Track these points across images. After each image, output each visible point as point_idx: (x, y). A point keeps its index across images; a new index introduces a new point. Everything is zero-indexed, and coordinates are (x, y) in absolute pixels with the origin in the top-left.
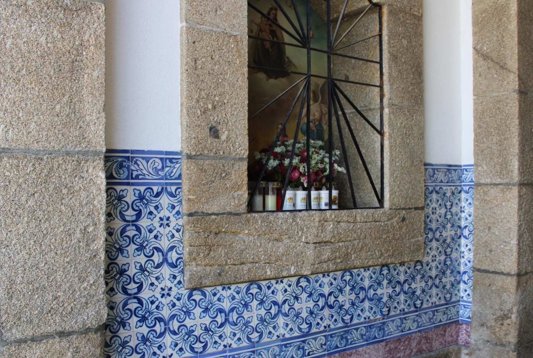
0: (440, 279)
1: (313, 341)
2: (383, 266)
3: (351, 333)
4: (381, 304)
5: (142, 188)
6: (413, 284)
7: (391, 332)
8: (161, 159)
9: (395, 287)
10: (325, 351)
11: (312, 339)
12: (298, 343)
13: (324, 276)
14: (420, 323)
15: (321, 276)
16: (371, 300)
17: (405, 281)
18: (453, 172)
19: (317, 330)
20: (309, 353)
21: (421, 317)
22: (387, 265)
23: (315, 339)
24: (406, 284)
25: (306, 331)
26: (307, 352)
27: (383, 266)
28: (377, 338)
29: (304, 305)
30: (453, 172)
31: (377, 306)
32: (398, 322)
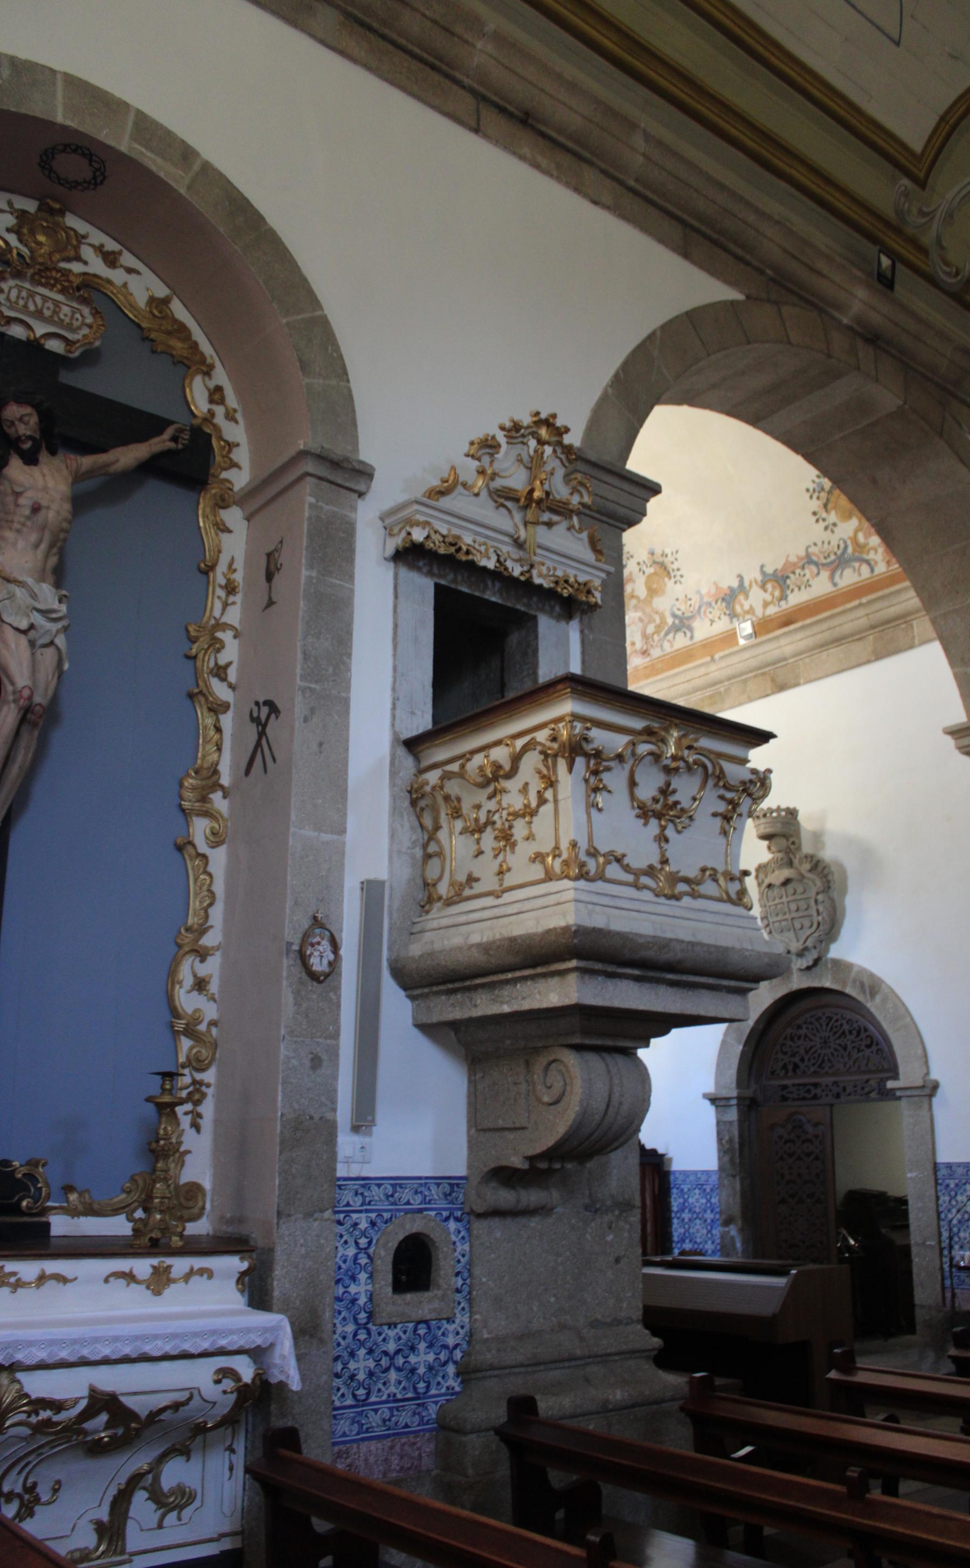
0: (344, 1364)
1: (373, 1413)
2: (419, 1322)
3: (366, 1416)
4: (415, 1378)
5: (373, 1215)
6: (352, 1362)
7: (372, 1427)
8: (392, 1185)
9: (439, 1353)
10: (389, 1429)
11: (372, 1410)
12: (352, 1415)
13: (389, 1328)
14: (365, 1427)
15: (386, 1327)
16: (399, 1369)
17: (398, 1352)
18: (374, 1188)
19: (378, 1399)
20: (367, 1429)
21: (426, 1409)
22: (426, 1322)
23: (376, 1411)
24: (400, 1357)
25: (421, 1391)
26: (426, 1419)
27: (419, 1322)
28: (347, 1436)
29: (361, 1365)
30: (374, 1188)
31: (348, 1386)
32: (387, 1414)
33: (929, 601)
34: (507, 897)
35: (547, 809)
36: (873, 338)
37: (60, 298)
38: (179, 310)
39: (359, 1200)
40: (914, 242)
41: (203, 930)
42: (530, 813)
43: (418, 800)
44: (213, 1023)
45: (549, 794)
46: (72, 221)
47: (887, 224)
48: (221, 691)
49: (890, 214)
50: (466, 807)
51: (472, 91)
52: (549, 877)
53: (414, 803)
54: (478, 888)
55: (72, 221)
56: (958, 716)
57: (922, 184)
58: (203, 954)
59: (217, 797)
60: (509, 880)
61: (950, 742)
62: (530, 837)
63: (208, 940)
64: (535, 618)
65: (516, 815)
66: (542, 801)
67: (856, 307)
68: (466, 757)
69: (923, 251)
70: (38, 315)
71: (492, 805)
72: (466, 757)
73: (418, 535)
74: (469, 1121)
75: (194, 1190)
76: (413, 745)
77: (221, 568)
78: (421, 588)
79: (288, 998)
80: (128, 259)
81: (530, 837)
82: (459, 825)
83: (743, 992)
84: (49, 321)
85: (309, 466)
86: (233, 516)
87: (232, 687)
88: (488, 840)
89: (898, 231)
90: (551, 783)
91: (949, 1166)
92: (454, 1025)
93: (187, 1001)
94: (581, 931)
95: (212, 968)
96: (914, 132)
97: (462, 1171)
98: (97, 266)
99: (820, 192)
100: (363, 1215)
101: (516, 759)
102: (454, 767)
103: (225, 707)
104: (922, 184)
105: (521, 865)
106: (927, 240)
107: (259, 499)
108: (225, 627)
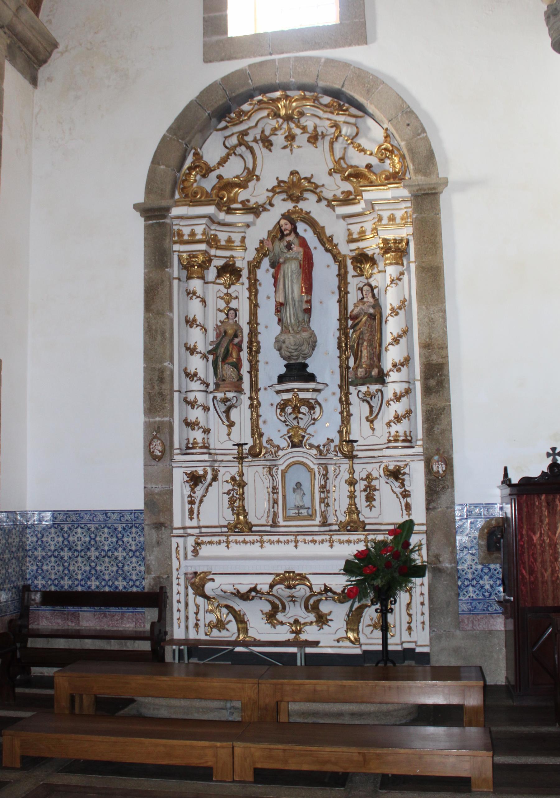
5: (124, 525)
8: (94, 521)
39: (136, 515)
100: (93, 525)
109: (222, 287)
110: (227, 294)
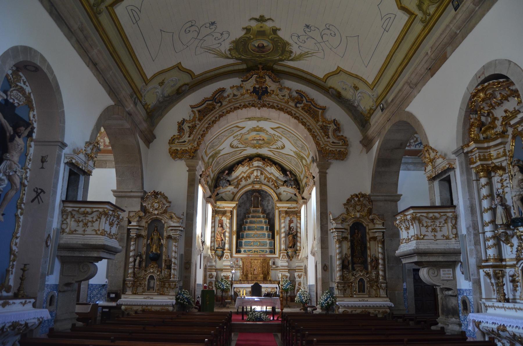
33: (117, 162)
34: (86, 236)
35: (98, 222)
36: (130, 114)
37: (21, 95)
38: (32, 97)
40: (141, 95)
41: (17, 233)
42: (93, 222)
43: (63, 212)
44: (17, 252)
45: (99, 220)
46: (20, 74)
47: (138, 90)
48: (26, 183)
49: (140, 89)
50: (75, 217)
51: (89, 58)
52: (97, 234)
53: (62, 212)
54: (77, 232)
55: (20, 74)
56: (115, 188)
57: (146, 85)
58: (17, 238)
59: (22, 205)
60: (86, 233)
61: (112, 193)
62: (92, 226)
63: (18, 235)
64: (79, 176)
65: (90, 221)
66: (97, 220)
67: (130, 108)
68: (80, 208)
69: (142, 97)
70: (17, 98)
71: (84, 218)
72: (80, 208)
73: (74, 161)
74: (60, 273)
75: (10, 286)
76: (63, 201)
77: (29, 156)
78: (68, 168)
79: (44, 249)
80: (27, 84)
81: (92, 226)
82: (73, 219)
83: (115, 255)
84: (18, 100)
85: (59, 144)
86: (32, 144)
87: (28, 182)
88: (81, 224)
89: (140, 92)
90: (100, 218)
91: (92, 285)
92: (61, 256)
93: (14, 248)
94: (104, 245)
95: (18, 241)
96: (149, 76)
97: (58, 283)
98: (22, 84)
99: (131, 83)
101: (93, 212)
102: (77, 209)
103: (26, 186)
104: (146, 85)
105: (89, 230)
106: (143, 95)
107: (39, 143)
108: (28, 168)
109: (498, 177)
110: (501, 180)
